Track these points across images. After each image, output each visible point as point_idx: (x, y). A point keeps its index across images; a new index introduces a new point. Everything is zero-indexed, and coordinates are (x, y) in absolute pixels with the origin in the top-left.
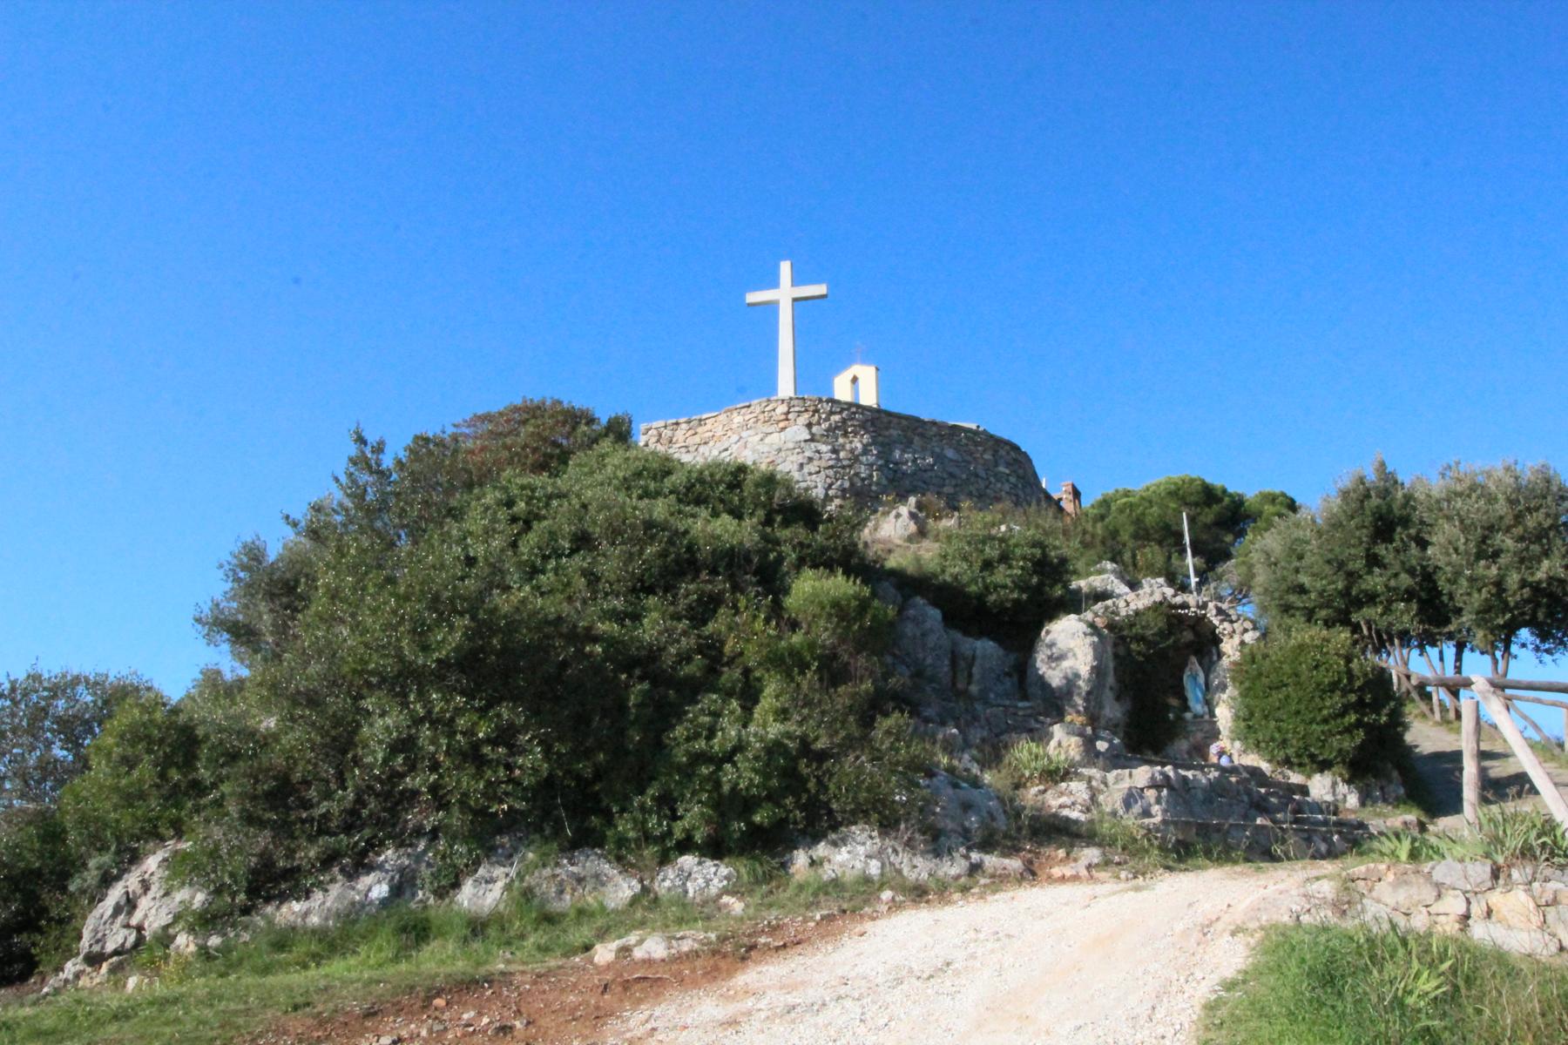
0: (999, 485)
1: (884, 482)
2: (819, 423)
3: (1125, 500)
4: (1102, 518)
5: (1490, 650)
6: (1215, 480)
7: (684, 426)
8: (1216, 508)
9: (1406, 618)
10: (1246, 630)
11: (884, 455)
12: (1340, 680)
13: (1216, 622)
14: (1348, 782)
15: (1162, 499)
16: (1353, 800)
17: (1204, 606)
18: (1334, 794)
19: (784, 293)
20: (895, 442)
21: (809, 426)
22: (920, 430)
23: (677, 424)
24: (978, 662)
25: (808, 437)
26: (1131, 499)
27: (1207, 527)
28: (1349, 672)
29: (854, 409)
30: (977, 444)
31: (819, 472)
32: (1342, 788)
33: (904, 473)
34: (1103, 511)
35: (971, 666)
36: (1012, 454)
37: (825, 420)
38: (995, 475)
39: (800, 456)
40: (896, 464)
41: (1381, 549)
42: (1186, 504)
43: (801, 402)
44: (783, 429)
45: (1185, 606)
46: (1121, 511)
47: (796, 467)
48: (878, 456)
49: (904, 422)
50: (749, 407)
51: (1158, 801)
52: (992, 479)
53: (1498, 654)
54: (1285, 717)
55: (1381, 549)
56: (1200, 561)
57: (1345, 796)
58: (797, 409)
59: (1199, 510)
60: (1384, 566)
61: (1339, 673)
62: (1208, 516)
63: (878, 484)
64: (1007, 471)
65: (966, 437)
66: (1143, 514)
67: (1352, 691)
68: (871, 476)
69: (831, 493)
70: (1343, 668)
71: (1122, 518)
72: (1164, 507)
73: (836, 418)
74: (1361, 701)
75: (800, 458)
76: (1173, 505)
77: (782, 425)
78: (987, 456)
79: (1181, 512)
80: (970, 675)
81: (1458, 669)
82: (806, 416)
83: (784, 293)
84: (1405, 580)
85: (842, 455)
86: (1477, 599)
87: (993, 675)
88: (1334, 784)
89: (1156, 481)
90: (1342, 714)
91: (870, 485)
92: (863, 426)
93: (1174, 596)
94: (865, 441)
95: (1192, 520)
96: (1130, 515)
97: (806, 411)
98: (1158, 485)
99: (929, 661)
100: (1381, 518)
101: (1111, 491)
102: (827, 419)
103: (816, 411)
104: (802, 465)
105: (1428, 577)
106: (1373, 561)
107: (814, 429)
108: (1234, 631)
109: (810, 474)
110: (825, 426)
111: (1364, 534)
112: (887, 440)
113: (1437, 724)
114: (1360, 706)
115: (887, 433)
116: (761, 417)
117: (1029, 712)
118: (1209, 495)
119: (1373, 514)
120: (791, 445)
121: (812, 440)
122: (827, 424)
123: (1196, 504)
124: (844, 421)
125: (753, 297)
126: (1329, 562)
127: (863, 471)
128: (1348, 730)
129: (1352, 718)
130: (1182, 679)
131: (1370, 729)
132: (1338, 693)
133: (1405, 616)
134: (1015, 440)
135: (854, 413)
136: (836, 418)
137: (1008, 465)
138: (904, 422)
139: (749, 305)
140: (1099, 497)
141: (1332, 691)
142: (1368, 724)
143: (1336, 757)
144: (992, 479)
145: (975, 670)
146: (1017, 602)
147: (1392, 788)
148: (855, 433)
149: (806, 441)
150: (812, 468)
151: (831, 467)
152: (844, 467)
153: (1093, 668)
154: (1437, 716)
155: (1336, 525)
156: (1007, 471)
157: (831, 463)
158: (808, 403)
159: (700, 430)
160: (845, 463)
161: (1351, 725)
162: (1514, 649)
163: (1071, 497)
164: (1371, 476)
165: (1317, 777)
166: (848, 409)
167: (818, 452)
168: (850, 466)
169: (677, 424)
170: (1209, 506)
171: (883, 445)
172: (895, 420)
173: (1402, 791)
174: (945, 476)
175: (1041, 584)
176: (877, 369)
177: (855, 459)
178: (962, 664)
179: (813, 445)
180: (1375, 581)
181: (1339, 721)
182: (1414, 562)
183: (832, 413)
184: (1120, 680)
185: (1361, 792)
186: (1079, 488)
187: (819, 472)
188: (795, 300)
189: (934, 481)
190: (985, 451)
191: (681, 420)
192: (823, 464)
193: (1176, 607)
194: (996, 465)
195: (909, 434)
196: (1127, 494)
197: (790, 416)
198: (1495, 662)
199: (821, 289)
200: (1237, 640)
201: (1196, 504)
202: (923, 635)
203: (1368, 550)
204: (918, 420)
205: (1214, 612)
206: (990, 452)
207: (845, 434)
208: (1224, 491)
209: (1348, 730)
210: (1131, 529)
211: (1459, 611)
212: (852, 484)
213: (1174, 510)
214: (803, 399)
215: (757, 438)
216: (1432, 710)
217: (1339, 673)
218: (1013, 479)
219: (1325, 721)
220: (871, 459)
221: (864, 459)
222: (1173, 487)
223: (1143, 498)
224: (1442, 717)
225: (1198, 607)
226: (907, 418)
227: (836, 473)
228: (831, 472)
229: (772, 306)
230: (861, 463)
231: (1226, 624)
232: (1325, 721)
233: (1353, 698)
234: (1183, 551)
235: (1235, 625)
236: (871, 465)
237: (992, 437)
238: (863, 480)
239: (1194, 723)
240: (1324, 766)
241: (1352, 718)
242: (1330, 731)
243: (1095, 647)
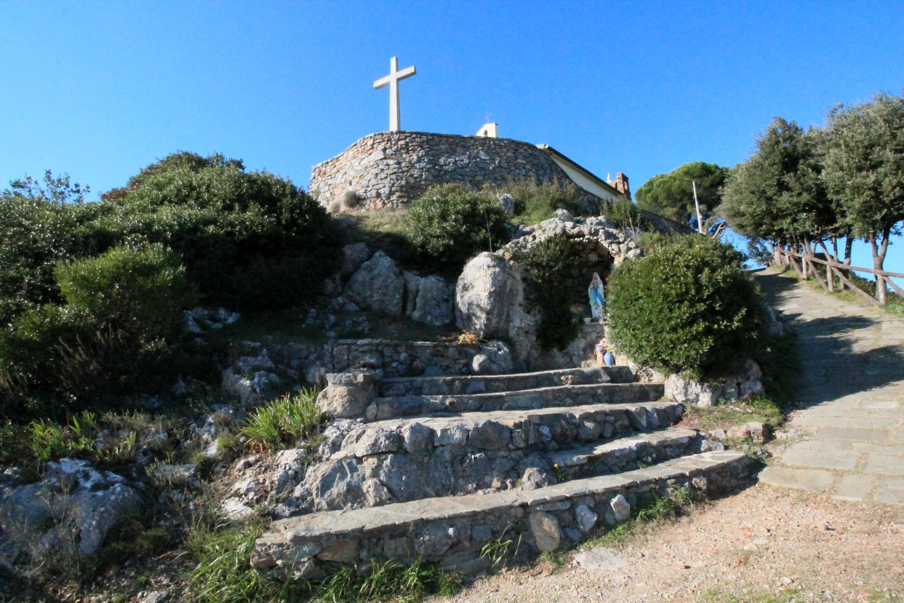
0: (517, 171)
1: (431, 178)
2: (391, 148)
3: (661, 179)
4: (650, 191)
5: (870, 237)
6: (710, 162)
7: (330, 164)
8: (711, 177)
9: (808, 223)
10: (629, 249)
11: (434, 162)
12: (687, 292)
13: (605, 244)
14: (701, 381)
15: (681, 176)
16: (705, 399)
17: (596, 233)
18: (686, 394)
19: (392, 78)
20: (443, 153)
21: (384, 150)
22: (461, 143)
23: (327, 163)
24: (420, 293)
25: (382, 157)
26: (664, 179)
27: (706, 189)
28: (697, 282)
29: (414, 136)
30: (501, 147)
31: (386, 177)
32: (695, 388)
33: (446, 172)
34: (649, 187)
35: (415, 297)
36: (530, 151)
37: (394, 145)
38: (515, 165)
39: (376, 170)
40: (442, 166)
41: (788, 178)
42: (694, 178)
43: (380, 136)
44: (370, 154)
45: (581, 234)
46: (659, 186)
47: (374, 176)
48: (428, 163)
49: (451, 140)
50: (356, 145)
51: (375, 473)
52: (512, 168)
53: (878, 242)
54: (639, 326)
55: (788, 178)
56: (703, 207)
57: (698, 395)
58: (378, 141)
59: (702, 179)
60: (788, 189)
61: (686, 284)
62: (707, 182)
63: (426, 180)
64: (524, 162)
65: (494, 144)
66: (671, 186)
67: (701, 300)
68: (421, 175)
69: (393, 189)
70: (690, 279)
71: (660, 189)
72: (682, 181)
73: (402, 142)
74: (711, 310)
75: (376, 171)
76: (686, 179)
77: (369, 152)
78: (509, 154)
79: (691, 182)
80: (415, 304)
81: (848, 255)
82: (383, 144)
83: (392, 78)
84: (806, 197)
85: (403, 164)
86: (857, 203)
87: (433, 302)
88: (686, 387)
89: (677, 168)
90: (692, 321)
91: (420, 181)
92: (421, 145)
93: (573, 228)
94: (420, 154)
95: (698, 186)
96: (663, 187)
97: (384, 141)
98: (679, 170)
99: (376, 297)
100: (788, 156)
101: (654, 177)
102: (396, 144)
103: (389, 140)
104: (377, 175)
105: (821, 192)
106: (782, 187)
107: (388, 152)
108: (620, 250)
109: (382, 179)
110: (394, 148)
111: (775, 170)
112: (436, 153)
113: (829, 293)
114: (709, 314)
115: (437, 148)
116: (360, 150)
117: (366, 348)
118: (706, 170)
119: (782, 154)
120: (372, 164)
121: (385, 158)
122: (396, 147)
123: (700, 177)
124: (407, 144)
125: (377, 83)
126: (753, 193)
127: (416, 173)
128: (697, 337)
129: (701, 326)
130: (587, 289)
131: (719, 335)
132: (686, 303)
133: (806, 223)
134: (532, 143)
135: (414, 138)
136: (402, 142)
137: (525, 158)
138: (451, 140)
139: (377, 88)
140: (648, 181)
141: (681, 302)
142: (719, 330)
143: (684, 363)
144: (512, 168)
145: (418, 300)
146: (447, 246)
147: (746, 385)
148: (414, 150)
149: (381, 159)
150: (383, 175)
151: (395, 173)
152: (403, 172)
153: (491, 294)
154: (830, 288)
155: (758, 166)
156: (524, 162)
157: (395, 170)
158: (385, 136)
159: (337, 164)
160: (404, 169)
161: (698, 333)
162: (892, 237)
163: (621, 181)
164: (776, 125)
165: (673, 377)
166: (410, 136)
167: (388, 165)
168: (407, 171)
169: (327, 163)
170: (707, 176)
171: (434, 156)
172: (445, 139)
173: (759, 387)
174: (477, 170)
175: (468, 232)
176: (496, 124)
177: (412, 166)
178: (411, 296)
179: (385, 161)
180: (785, 200)
181: (687, 329)
182: (810, 183)
183: (399, 140)
184: (527, 298)
185: (714, 390)
186: (626, 175)
187: (386, 177)
188: (399, 80)
189: (469, 174)
190: (508, 151)
191: (329, 161)
192: (390, 172)
193: (573, 236)
194: (516, 158)
195: (454, 147)
196: (662, 176)
197: (375, 146)
198: (876, 247)
199: (411, 70)
200: (622, 256)
201: (700, 177)
202: (372, 279)
203: (778, 180)
204: (461, 137)
205: (603, 237)
206: (512, 151)
207: (407, 152)
208: (717, 167)
209: (697, 337)
210: (665, 195)
211: (843, 214)
212: (407, 182)
213: (688, 181)
214: (382, 134)
215: (358, 163)
216: (827, 283)
217: (686, 284)
218: (528, 167)
219: (674, 329)
220: (422, 165)
221: (417, 165)
222: (686, 169)
223: (670, 177)
224: (834, 287)
225: (590, 234)
226: (452, 137)
227: (397, 176)
228: (394, 177)
229: (386, 86)
230: (416, 168)
231: (614, 246)
232: (674, 329)
233: (701, 307)
234: (693, 204)
235: (621, 246)
236: (422, 169)
237: (513, 141)
238: (416, 178)
239: (590, 326)
240: (677, 369)
241: (701, 326)
242: (678, 339)
243: (495, 276)
